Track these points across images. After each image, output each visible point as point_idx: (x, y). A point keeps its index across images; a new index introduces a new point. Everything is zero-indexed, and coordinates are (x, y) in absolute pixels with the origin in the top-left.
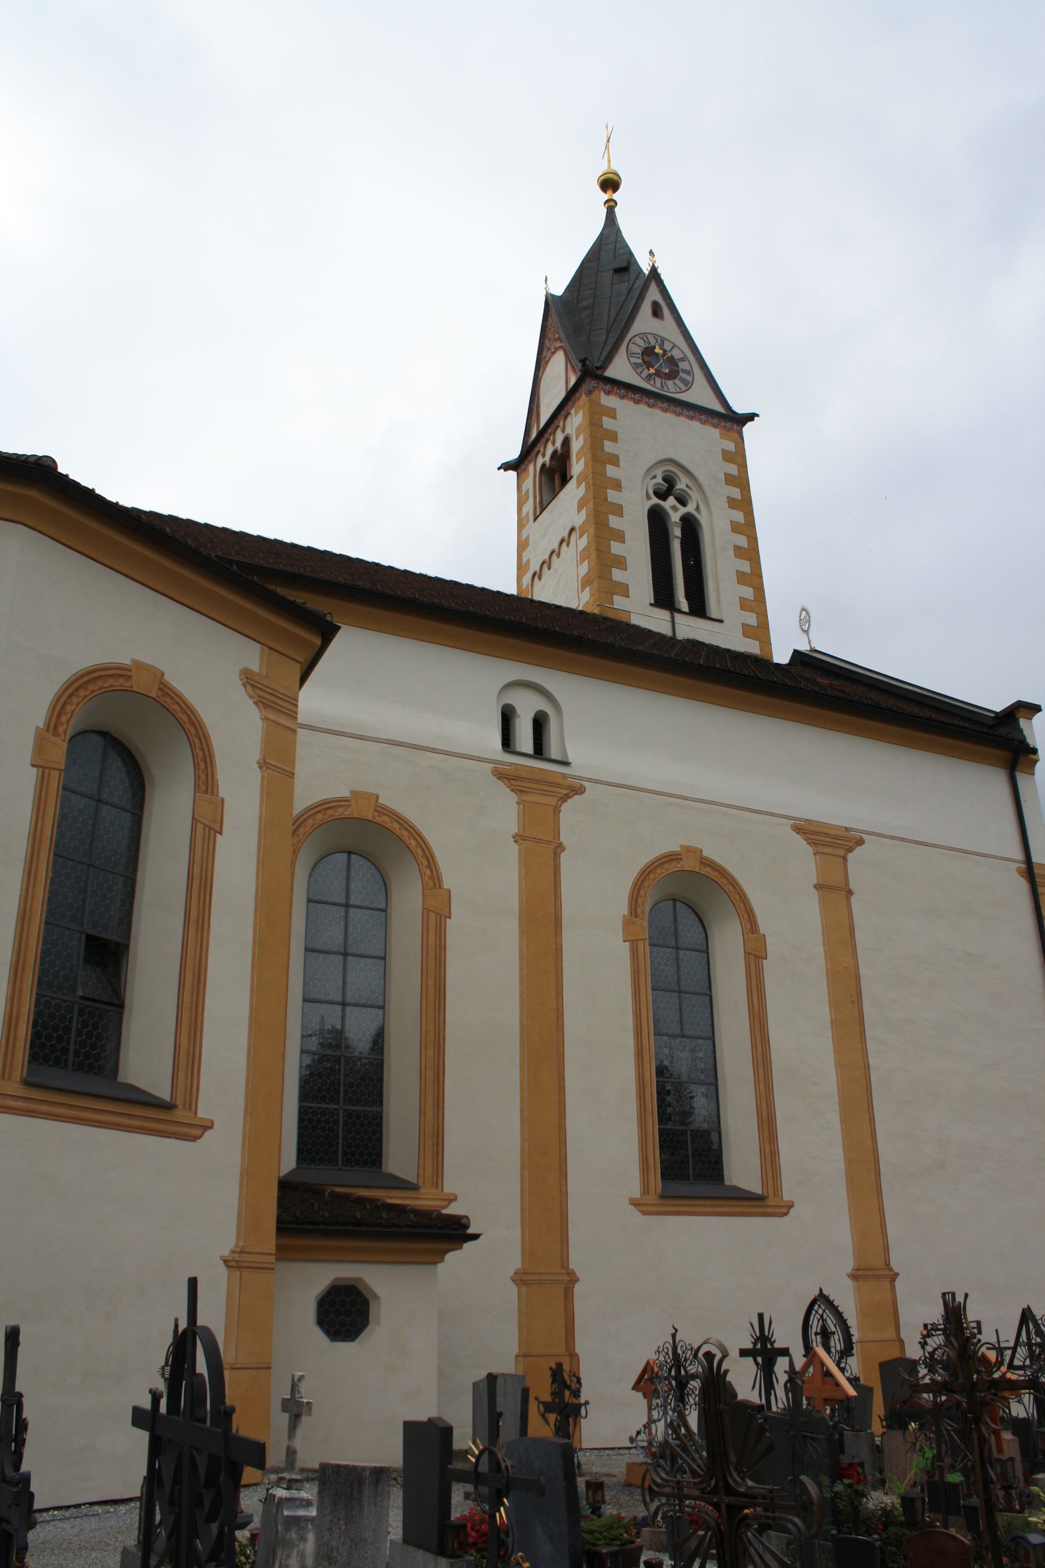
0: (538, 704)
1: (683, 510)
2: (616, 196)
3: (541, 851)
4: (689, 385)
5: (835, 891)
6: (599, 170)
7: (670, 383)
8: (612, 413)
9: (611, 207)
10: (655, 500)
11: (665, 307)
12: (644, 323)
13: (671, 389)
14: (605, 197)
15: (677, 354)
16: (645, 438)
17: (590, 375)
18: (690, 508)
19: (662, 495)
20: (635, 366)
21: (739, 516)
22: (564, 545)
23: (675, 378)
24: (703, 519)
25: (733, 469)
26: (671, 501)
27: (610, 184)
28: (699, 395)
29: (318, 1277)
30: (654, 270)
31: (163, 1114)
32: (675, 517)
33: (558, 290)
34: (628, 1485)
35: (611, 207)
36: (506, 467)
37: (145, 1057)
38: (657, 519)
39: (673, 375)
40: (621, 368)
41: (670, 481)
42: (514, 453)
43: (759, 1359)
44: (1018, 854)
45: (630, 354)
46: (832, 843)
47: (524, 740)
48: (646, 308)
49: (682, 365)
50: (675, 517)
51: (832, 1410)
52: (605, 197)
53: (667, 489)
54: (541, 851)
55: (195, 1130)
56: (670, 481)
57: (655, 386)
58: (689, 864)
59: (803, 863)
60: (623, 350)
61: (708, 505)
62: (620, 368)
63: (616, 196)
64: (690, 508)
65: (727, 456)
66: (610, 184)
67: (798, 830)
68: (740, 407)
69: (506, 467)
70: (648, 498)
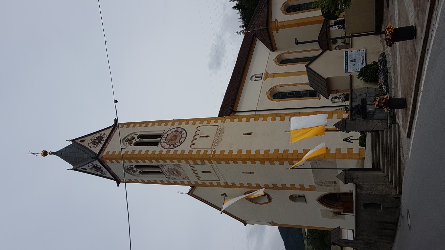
1: (136, 138)
4: (104, 134)
7: (103, 139)
9: (52, 153)
10: (133, 144)
11: (82, 139)
12: (85, 144)
13: (104, 138)
14: (49, 155)
16: (115, 146)
20: (97, 146)
21: (191, 123)
22: (200, 179)
23: (101, 138)
24: (139, 134)
25: (157, 124)
27: (45, 154)
28: (108, 132)
30: (72, 141)
32: (138, 140)
35: (52, 153)
38: (137, 144)
40: (97, 150)
41: (128, 141)
45: (94, 147)
48: (82, 143)
50: (138, 140)
52: (49, 155)
53: (130, 141)
56: (128, 141)
57: (103, 142)
60: (91, 149)
61: (135, 133)
62: (97, 150)
64: (136, 136)
65: (209, 122)
66: (45, 154)
68: (112, 123)
70: (132, 146)
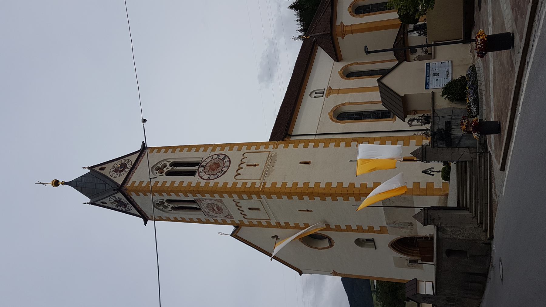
1: (168, 166)
2: (61, 181)
3: (338, 91)
9: (64, 183)
10: (164, 174)
12: (106, 172)
13: (129, 166)
14: (61, 185)
16: (142, 175)
23: (126, 165)
24: (172, 161)
27: (56, 183)
28: (134, 158)
32: (170, 168)
34: (426, 35)
35: (64, 183)
36: (145, 223)
38: (169, 174)
40: (119, 180)
41: (158, 169)
42: (141, 220)
45: (116, 177)
48: (102, 172)
50: (170, 168)
52: (61, 185)
53: (160, 170)
54: (338, 91)
56: (158, 169)
57: (127, 170)
58: (351, 9)
60: (113, 179)
63: (61, 181)
64: (168, 164)
66: (56, 183)
68: (139, 147)
69: (145, 223)
70: (163, 175)
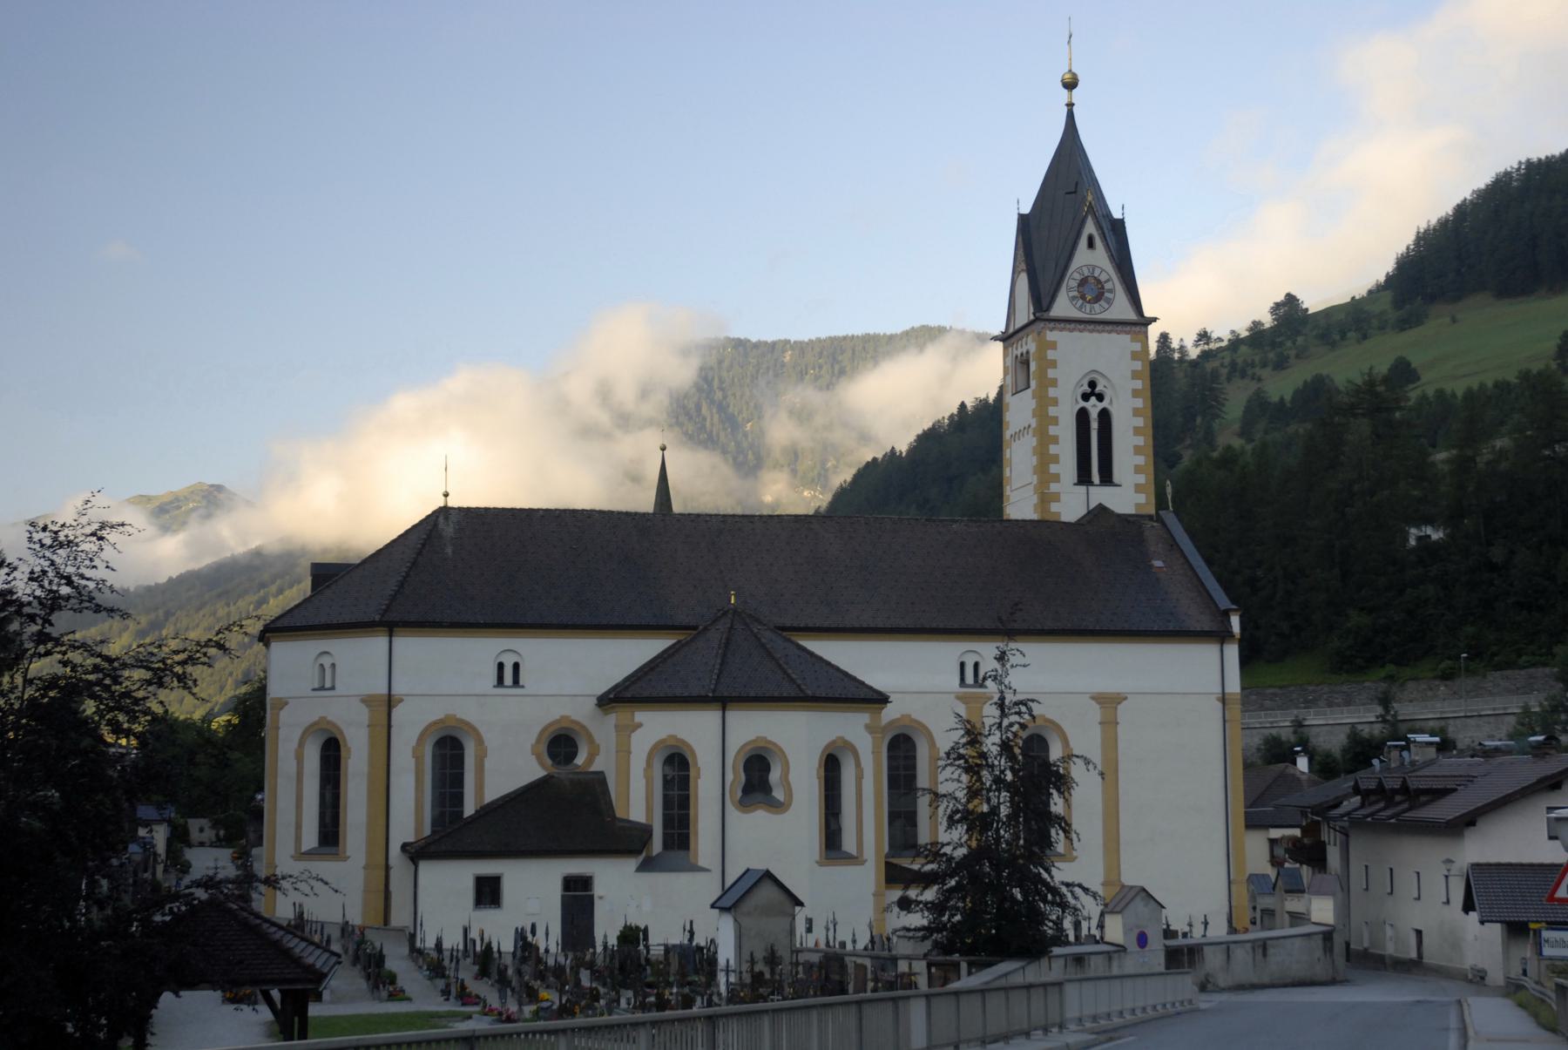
0: (975, 658)
1: (1101, 406)
5: (1109, 725)
6: (1061, 71)
8: (1053, 346)
10: (1082, 404)
15: (1103, 278)
17: (1041, 299)
18: (1105, 404)
19: (1086, 397)
26: (1093, 399)
27: (1071, 84)
29: (896, 894)
31: (854, 860)
33: (1026, 209)
37: (849, 844)
38: (1082, 416)
39: (1098, 298)
41: (1092, 384)
43: (276, 994)
44: (1219, 690)
46: (1109, 702)
47: (970, 679)
48: (1083, 242)
49: (1107, 286)
51: (62, 926)
53: (1092, 391)
55: (863, 862)
59: (1095, 712)
64: (1105, 404)
67: (1093, 698)
